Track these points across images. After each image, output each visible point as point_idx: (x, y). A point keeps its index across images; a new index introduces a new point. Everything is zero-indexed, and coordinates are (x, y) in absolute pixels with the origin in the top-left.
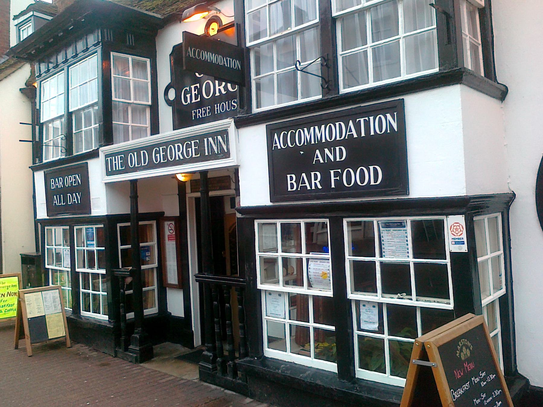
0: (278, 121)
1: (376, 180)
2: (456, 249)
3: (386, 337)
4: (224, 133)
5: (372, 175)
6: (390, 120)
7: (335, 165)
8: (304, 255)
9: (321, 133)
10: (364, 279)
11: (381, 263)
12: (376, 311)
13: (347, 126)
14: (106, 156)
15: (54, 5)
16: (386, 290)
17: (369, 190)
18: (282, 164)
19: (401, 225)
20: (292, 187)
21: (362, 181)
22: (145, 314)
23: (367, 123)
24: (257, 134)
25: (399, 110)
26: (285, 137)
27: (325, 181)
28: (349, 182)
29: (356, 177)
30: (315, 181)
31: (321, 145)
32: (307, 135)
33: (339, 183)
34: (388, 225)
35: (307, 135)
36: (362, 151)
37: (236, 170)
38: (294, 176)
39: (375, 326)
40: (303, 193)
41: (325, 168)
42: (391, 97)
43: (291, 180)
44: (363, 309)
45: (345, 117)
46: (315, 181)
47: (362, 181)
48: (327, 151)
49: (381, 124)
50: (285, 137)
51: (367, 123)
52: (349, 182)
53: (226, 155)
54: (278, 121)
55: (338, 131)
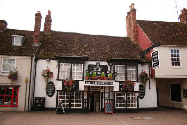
0: (120, 82)
4: (112, 82)
43: (122, 89)
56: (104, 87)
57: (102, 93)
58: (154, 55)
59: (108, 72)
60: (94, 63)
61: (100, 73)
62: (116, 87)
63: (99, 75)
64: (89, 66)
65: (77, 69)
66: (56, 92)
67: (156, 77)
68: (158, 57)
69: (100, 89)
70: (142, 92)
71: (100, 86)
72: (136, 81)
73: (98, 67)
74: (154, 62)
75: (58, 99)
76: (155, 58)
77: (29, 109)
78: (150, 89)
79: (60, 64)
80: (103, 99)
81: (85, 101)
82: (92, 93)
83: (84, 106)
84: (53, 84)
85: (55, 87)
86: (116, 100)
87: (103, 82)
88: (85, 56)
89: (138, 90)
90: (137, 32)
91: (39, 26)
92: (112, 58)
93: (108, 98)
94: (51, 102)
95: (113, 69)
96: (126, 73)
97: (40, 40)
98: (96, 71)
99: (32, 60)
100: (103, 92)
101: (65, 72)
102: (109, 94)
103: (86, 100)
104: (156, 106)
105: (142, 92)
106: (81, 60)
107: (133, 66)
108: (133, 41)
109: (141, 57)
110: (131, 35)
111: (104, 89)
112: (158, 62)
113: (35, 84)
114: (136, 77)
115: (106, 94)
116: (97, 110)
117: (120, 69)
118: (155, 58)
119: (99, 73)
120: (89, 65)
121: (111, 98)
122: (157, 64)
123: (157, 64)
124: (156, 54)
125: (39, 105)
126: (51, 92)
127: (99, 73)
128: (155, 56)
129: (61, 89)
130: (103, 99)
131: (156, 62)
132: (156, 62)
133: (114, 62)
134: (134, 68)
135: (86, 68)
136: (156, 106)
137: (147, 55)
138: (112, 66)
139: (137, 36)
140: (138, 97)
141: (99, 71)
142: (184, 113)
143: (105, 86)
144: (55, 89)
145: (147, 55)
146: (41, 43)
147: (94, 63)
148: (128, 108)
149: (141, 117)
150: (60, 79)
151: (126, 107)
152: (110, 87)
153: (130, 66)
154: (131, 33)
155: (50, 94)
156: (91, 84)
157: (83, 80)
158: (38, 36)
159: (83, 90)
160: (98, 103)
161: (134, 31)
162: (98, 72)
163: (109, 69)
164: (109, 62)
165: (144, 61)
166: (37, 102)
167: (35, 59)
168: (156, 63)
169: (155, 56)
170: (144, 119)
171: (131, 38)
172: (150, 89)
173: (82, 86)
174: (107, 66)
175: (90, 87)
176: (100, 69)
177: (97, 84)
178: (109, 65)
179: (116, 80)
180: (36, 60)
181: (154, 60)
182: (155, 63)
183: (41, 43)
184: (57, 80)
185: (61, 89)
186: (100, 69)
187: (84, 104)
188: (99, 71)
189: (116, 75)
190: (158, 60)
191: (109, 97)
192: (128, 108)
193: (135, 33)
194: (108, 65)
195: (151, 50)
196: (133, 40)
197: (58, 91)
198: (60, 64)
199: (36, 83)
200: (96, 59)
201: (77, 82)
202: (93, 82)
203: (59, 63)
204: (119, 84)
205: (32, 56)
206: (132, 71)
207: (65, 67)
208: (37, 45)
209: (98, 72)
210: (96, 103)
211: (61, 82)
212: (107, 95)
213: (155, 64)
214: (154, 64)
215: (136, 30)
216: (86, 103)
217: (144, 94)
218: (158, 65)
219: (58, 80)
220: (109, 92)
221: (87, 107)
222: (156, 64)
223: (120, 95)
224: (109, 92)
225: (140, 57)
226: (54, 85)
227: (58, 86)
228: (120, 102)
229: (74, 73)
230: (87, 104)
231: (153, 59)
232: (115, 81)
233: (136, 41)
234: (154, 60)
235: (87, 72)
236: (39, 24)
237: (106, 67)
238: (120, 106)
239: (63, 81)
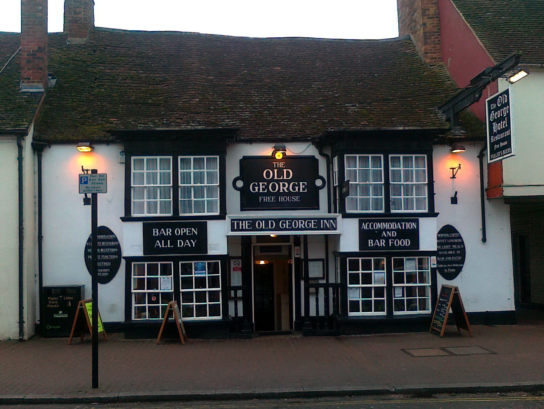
0: (363, 218)
1: (408, 244)
2: (433, 266)
3: (405, 298)
4: (334, 219)
5: (406, 242)
6: (414, 225)
7: (392, 238)
8: (159, 276)
9: (386, 226)
10: (399, 278)
11: (371, 273)
12: (401, 290)
13: (397, 224)
14: (232, 220)
15: (402, 38)
16: (420, 282)
17: (405, 247)
18: (364, 236)
19: (414, 259)
20: (371, 244)
21: (402, 244)
22: (323, 315)
23: (405, 225)
24: (355, 222)
25: (417, 222)
26: (368, 225)
27: (387, 243)
28: (397, 244)
29: (400, 243)
30: (383, 243)
31: (386, 230)
32: (379, 226)
33: (393, 245)
34: (408, 260)
35: (379, 226)
36: (402, 234)
37: (339, 236)
38: (384, 241)
39: (401, 295)
40: (377, 247)
41: (387, 239)
42: (415, 218)
43: (371, 243)
44: (396, 290)
45: (397, 221)
46: (383, 243)
47: (402, 244)
48: (388, 232)
49: (410, 226)
50: (368, 225)
51: (405, 225)
52: (397, 244)
53: (335, 229)
54: (363, 218)
55: (393, 226)
56: (302, 240)
57: (298, 260)
58: (497, 109)
59: (319, 183)
60: (266, 150)
61: (288, 189)
62: (349, 237)
63: (284, 194)
64: (246, 162)
65: (365, 175)
66: (123, 262)
67: (508, 192)
68: (508, 115)
69: (290, 248)
70: (451, 252)
71: (288, 236)
72: (426, 211)
73: (281, 165)
74: (495, 135)
75: (133, 291)
76: (498, 120)
77: (26, 326)
78: (484, 240)
79: (133, 158)
80: (302, 283)
81: (240, 293)
82: (262, 262)
83: (232, 313)
84: (113, 234)
85: (118, 247)
86: (181, 290)
87: (298, 219)
88: (227, 122)
89: (434, 248)
90: (438, 16)
91: (41, 11)
92: (330, 129)
93: (322, 278)
94: (111, 301)
95: (336, 169)
96: (176, 187)
97: (49, 67)
98: (273, 180)
99: (20, 148)
100: (302, 257)
101: (152, 193)
102: (325, 263)
103: (236, 289)
104: (510, 306)
105: (451, 252)
106: (213, 142)
107: (357, 156)
108: (421, 54)
109: (448, 120)
110: (414, 32)
111: (302, 245)
112: (507, 133)
113: (40, 237)
114: (427, 196)
115: (311, 264)
116: (285, 326)
117: (361, 171)
118: (498, 120)
119: (284, 185)
120: (245, 158)
121: (332, 280)
122: (506, 143)
123: (506, 143)
124: (502, 104)
125: (60, 315)
126: (106, 264)
127: (284, 185)
128: (499, 114)
129: (140, 254)
130: (302, 283)
131: (502, 136)
132: (502, 136)
133: (338, 142)
134: (352, 163)
135: (233, 171)
136: (510, 306)
137: (473, 109)
138: (333, 157)
139: (437, 33)
140: (433, 271)
141: (283, 180)
142: (381, 336)
143: (305, 236)
144: (119, 252)
145: (473, 109)
146: (53, 82)
147: (266, 150)
148: (396, 313)
149: (443, 349)
150: (134, 215)
151: (390, 312)
152: (326, 236)
153: (401, 156)
154: (413, 21)
155: (103, 273)
156: (255, 229)
157: (222, 217)
158: (38, 55)
159: (223, 251)
160: (284, 300)
161: (424, 12)
162: (278, 182)
163: (323, 172)
164: (319, 145)
165: (459, 132)
166: (53, 302)
167: (32, 144)
168: (502, 140)
169: (499, 114)
170: (452, 354)
171: (415, 42)
172: (484, 240)
173: (218, 239)
174: (312, 158)
175: (254, 241)
176: (288, 173)
177: (277, 229)
178: (321, 154)
179: (348, 211)
180: (39, 149)
181: (497, 127)
182: (497, 138)
183: (53, 82)
184: (123, 219)
185: (140, 254)
186: (288, 173)
187: (231, 305)
188: (283, 180)
189: (347, 194)
190: (508, 128)
191: (326, 275)
192: (396, 313)
193: (429, 22)
194: (318, 156)
195: (484, 86)
196: (420, 48)
197: (129, 260)
198: (133, 158)
199: (43, 234)
200: (271, 132)
201: (200, 225)
202: (262, 220)
203: (128, 153)
204: (360, 225)
205: (20, 135)
206: (199, 178)
207: (153, 172)
208: (38, 88)
209: (278, 182)
210: (279, 296)
211: (140, 225)
212: (315, 270)
213: (498, 142)
214: (492, 145)
215: (432, 11)
216: (236, 299)
217: (463, 261)
218: (509, 146)
219: (128, 218)
220: (324, 257)
221: (241, 314)
222: (502, 144)
223: (367, 265)
224: (324, 257)
225: (444, 118)
226: (116, 240)
227: (131, 240)
228: (201, 297)
229: (397, 190)
230: (240, 305)
231: (491, 123)
232: (346, 216)
233: (435, 55)
234: (497, 127)
235: (240, 184)
236: (39, 4)
237: (312, 160)
238: (201, 311)
239: (149, 225)
